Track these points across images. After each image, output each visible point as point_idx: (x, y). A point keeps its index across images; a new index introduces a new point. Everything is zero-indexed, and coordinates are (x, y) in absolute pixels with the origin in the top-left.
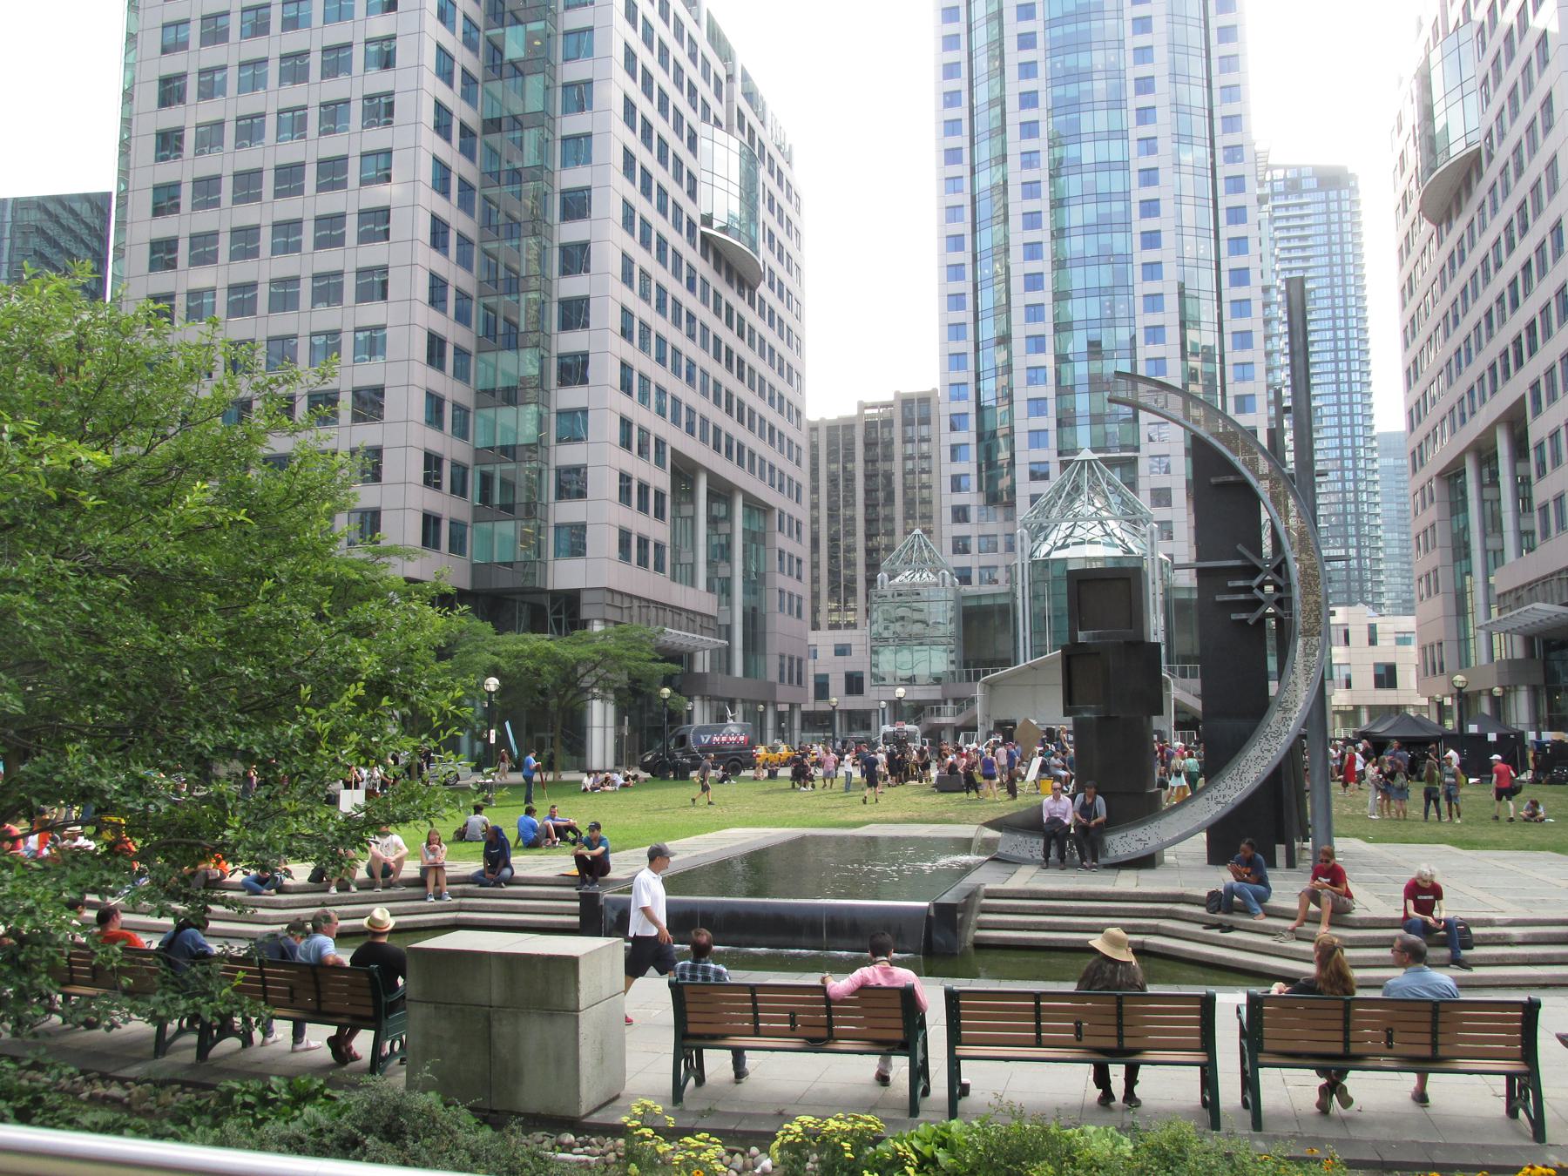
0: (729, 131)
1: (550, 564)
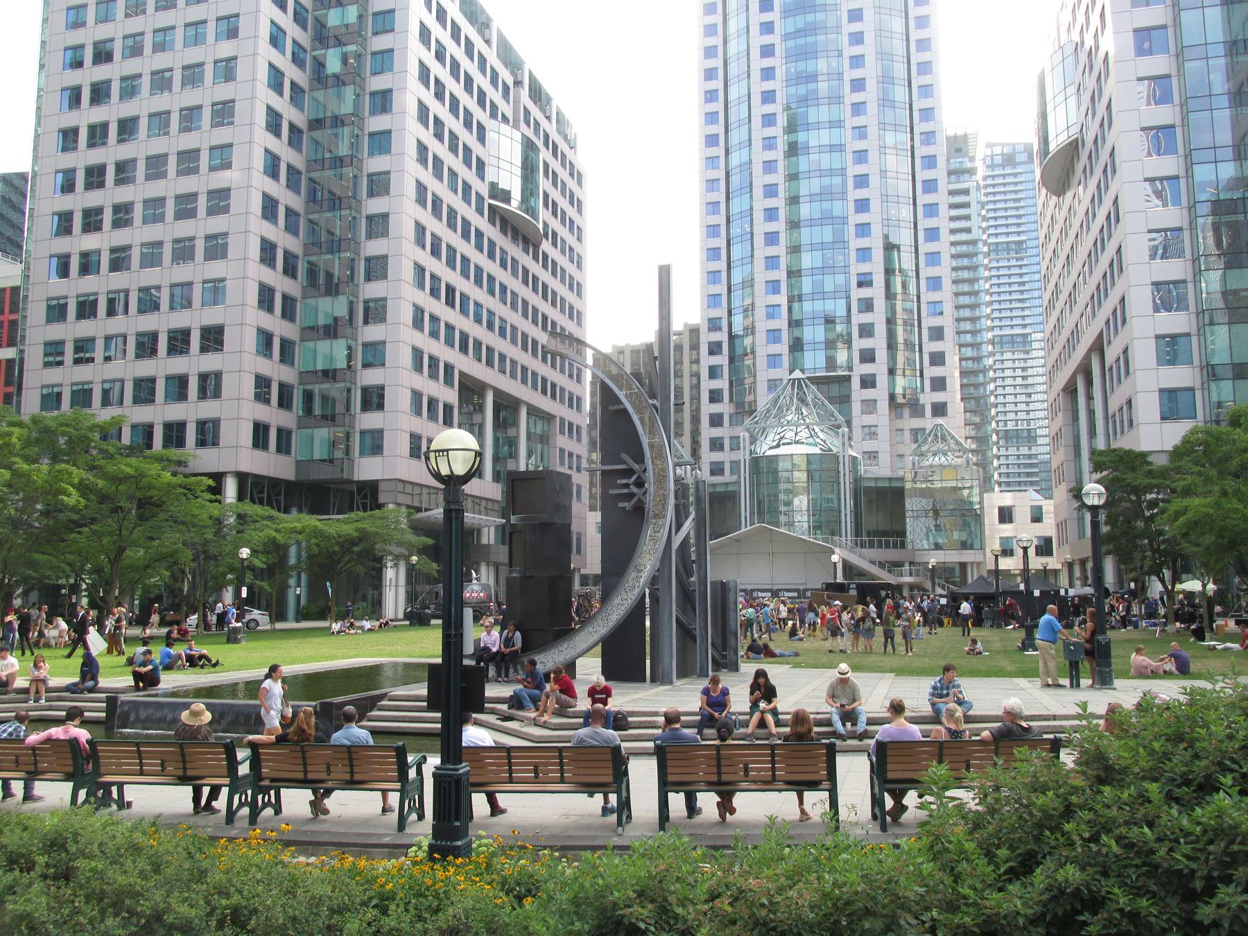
0: (516, 126)
1: (356, 461)
